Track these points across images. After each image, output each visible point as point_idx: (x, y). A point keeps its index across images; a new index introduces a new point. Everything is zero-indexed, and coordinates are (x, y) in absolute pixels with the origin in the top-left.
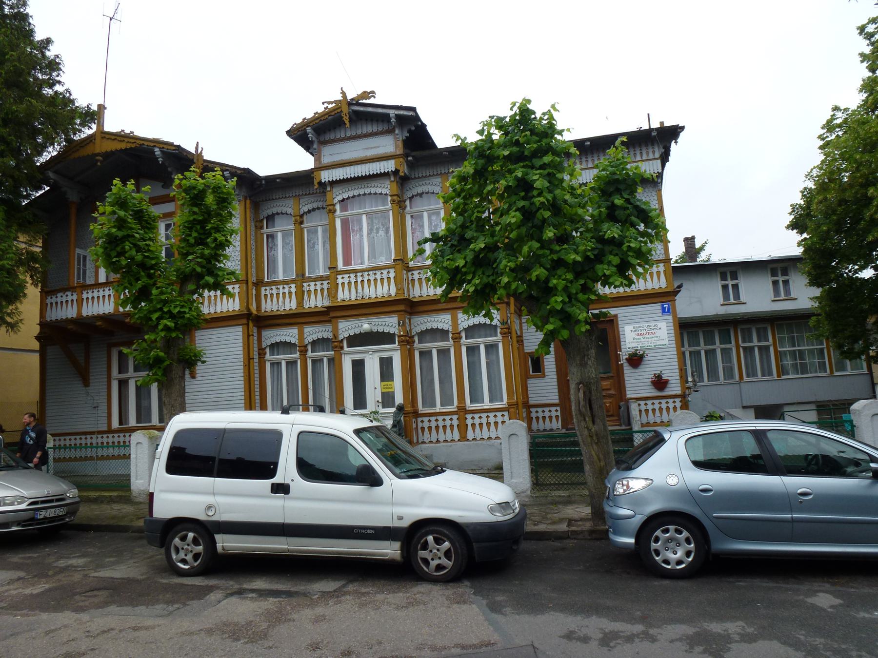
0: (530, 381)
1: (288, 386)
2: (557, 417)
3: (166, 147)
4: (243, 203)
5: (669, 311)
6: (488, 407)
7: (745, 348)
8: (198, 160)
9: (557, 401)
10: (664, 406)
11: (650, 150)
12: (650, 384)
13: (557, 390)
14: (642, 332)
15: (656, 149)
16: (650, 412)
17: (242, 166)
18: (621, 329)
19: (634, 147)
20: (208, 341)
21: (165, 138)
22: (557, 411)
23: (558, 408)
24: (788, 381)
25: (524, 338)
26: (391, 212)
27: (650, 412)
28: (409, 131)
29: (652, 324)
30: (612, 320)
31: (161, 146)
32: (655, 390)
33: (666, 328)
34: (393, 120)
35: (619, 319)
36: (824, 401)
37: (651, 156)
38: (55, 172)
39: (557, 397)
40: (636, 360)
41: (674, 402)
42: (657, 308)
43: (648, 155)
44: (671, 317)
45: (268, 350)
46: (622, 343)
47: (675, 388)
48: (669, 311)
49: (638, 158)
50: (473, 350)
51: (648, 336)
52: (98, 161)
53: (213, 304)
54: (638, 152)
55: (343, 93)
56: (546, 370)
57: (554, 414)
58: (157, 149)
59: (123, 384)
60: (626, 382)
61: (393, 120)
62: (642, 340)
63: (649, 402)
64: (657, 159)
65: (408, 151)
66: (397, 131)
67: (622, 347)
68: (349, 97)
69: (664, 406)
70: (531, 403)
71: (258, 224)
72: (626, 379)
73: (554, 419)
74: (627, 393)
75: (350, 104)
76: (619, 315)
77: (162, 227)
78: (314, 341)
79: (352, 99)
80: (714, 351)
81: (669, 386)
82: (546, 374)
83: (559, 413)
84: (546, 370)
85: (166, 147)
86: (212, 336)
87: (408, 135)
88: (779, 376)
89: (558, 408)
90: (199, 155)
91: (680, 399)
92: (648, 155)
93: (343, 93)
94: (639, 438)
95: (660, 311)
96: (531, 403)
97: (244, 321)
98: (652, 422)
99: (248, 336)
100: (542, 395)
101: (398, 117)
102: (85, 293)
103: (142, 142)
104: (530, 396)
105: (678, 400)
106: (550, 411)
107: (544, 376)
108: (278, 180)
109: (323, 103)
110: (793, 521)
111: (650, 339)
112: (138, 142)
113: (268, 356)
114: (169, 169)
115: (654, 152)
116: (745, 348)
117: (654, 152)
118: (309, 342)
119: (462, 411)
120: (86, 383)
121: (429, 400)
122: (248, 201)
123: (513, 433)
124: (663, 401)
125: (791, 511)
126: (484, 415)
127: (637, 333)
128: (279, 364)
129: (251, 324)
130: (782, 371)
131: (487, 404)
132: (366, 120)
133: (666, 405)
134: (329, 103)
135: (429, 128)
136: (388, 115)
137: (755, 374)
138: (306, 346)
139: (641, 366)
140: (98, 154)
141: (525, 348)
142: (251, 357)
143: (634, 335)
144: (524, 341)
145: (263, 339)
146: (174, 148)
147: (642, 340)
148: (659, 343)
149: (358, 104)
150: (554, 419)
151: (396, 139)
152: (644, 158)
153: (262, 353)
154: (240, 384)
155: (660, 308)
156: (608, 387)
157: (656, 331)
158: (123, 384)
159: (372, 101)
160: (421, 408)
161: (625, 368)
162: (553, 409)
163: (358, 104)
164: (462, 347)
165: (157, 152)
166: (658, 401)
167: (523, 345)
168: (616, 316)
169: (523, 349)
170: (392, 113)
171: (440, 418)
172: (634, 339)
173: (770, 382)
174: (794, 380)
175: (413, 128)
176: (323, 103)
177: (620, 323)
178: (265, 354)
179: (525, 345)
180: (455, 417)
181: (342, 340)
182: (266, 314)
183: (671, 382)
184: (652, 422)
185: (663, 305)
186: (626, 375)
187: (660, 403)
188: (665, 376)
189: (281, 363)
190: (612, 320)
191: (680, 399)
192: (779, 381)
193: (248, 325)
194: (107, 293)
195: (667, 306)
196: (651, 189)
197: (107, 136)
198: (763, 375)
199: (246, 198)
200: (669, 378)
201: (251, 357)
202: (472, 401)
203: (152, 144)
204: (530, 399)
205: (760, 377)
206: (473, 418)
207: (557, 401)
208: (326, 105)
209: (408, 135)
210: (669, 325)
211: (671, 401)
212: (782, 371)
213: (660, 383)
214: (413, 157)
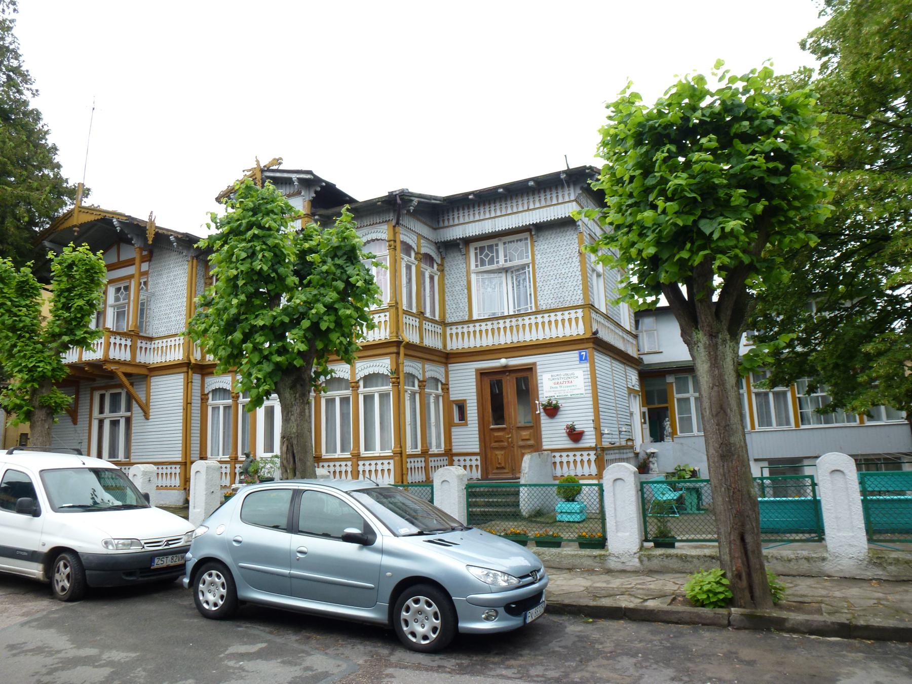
0: (454, 430)
1: (224, 428)
2: (477, 466)
3: (120, 217)
4: (190, 263)
5: (586, 359)
6: (378, 455)
7: (757, 394)
8: (151, 227)
9: (478, 450)
10: (578, 459)
11: (566, 193)
12: (566, 435)
13: (478, 439)
14: (559, 381)
15: (572, 191)
16: (565, 465)
17: (182, 231)
18: (539, 378)
19: (551, 190)
20: (159, 386)
21: (120, 211)
22: (477, 460)
23: (478, 458)
24: (807, 431)
25: (450, 386)
26: (388, 257)
27: (565, 465)
28: (316, 192)
29: (569, 372)
30: (532, 368)
31: (118, 217)
32: (571, 442)
33: (583, 377)
34: (296, 183)
35: (538, 367)
36: (869, 455)
37: (567, 199)
38: (51, 241)
39: (478, 446)
40: (552, 410)
41: (589, 455)
42: (574, 355)
43: (563, 198)
44: (588, 365)
45: (210, 396)
46: (540, 392)
47: (589, 440)
48: (586, 359)
49: (555, 202)
50: (368, 399)
51: (564, 385)
52: (75, 231)
53: (164, 354)
54: (554, 195)
55: (258, 161)
56: (469, 419)
57: (386, 467)
58: (114, 220)
59: (101, 422)
60: (543, 433)
61: (296, 183)
62: (559, 389)
63: (564, 454)
64: (573, 201)
65: (314, 210)
66: (303, 193)
67: (540, 396)
68: (262, 166)
69: (578, 459)
70: (454, 451)
71: (207, 281)
72: (543, 429)
73: (474, 467)
74: (544, 444)
75: (262, 171)
76: (538, 364)
77: (111, 291)
78: (365, 376)
79: (265, 166)
80: (688, 399)
81: (584, 437)
82: (469, 422)
83: (479, 463)
84: (469, 419)
85: (120, 217)
86: (162, 383)
87: (314, 195)
88: (797, 425)
89: (478, 458)
90: (152, 222)
91: (595, 452)
92: (563, 198)
93: (258, 161)
94: (524, 492)
95: (578, 359)
96: (454, 451)
97: (185, 369)
98: (587, 475)
99: (188, 383)
100: (464, 444)
101: (299, 180)
102: (113, 338)
103: (105, 214)
104: (453, 444)
105: (592, 453)
106: (471, 460)
107: (466, 425)
108: (587, 171)
109: (244, 171)
110: (291, 577)
111: (566, 389)
112: (102, 214)
113: (210, 401)
114: (129, 236)
115: (569, 195)
116: (757, 394)
117: (569, 195)
118: (361, 378)
119: (357, 457)
120: (75, 422)
121: (331, 448)
122: (195, 261)
123: (842, 469)
124: (578, 453)
125: (291, 567)
126: (373, 462)
127: (553, 381)
128: (333, 400)
129: (190, 372)
130: (802, 419)
131: (377, 452)
132: (282, 184)
133: (580, 458)
134: (248, 171)
135: (338, 187)
136: (291, 179)
137: (769, 424)
138: (358, 382)
139: (557, 417)
140: (75, 226)
141: (451, 396)
142: (189, 401)
143: (551, 383)
144: (450, 389)
145: (206, 386)
146: (125, 218)
147: (559, 389)
148: (575, 392)
149: (269, 170)
150: (474, 467)
151: (304, 201)
152: (560, 202)
153: (204, 398)
154: (180, 426)
155: (577, 355)
156: (527, 437)
157: (572, 380)
158: (101, 422)
159: (281, 167)
160: (324, 454)
161: (542, 418)
162: (474, 458)
163: (269, 170)
164: (360, 395)
165: (115, 222)
166: (573, 453)
167: (448, 393)
168: (535, 364)
169: (449, 397)
170: (294, 177)
171: (338, 464)
172: (551, 388)
173: (786, 432)
174: (814, 431)
175: (319, 189)
176: (244, 171)
177: (538, 371)
178: (208, 399)
179: (451, 393)
180: (349, 463)
181: (208, 394)
182: (210, 363)
183: (586, 433)
184: (587, 475)
185: (580, 353)
186: (542, 425)
187: (575, 455)
188: (579, 427)
189: (335, 399)
190: (532, 368)
191: (595, 452)
192: (861, 429)
193: (398, 353)
194: (123, 342)
195: (584, 353)
196: (572, 232)
197: (83, 210)
198: (779, 424)
199: (193, 259)
200: (585, 430)
201: (189, 401)
202: (366, 450)
203: (111, 216)
204: (453, 448)
205: (774, 427)
206: (364, 465)
207: (478, 450)
208: (246, 172)
209: (314, 195)
210: (586, 373)
211: (585, 453)
212: (802, 419)
213: (575, 435)
214: (319, 215)
